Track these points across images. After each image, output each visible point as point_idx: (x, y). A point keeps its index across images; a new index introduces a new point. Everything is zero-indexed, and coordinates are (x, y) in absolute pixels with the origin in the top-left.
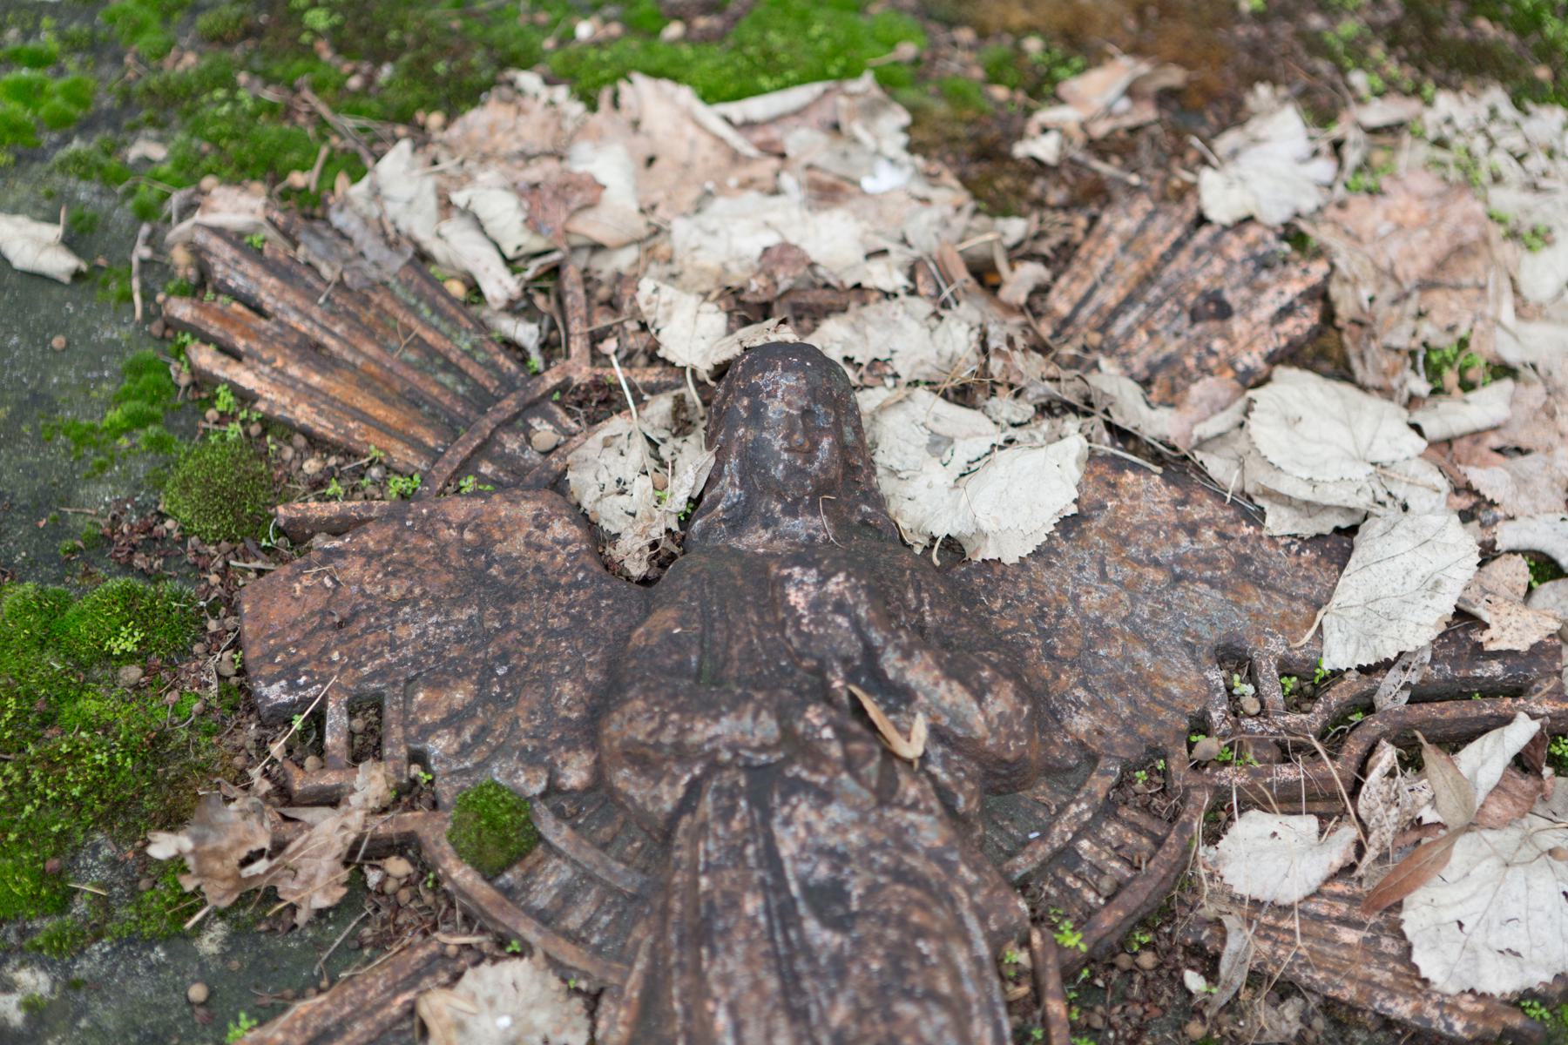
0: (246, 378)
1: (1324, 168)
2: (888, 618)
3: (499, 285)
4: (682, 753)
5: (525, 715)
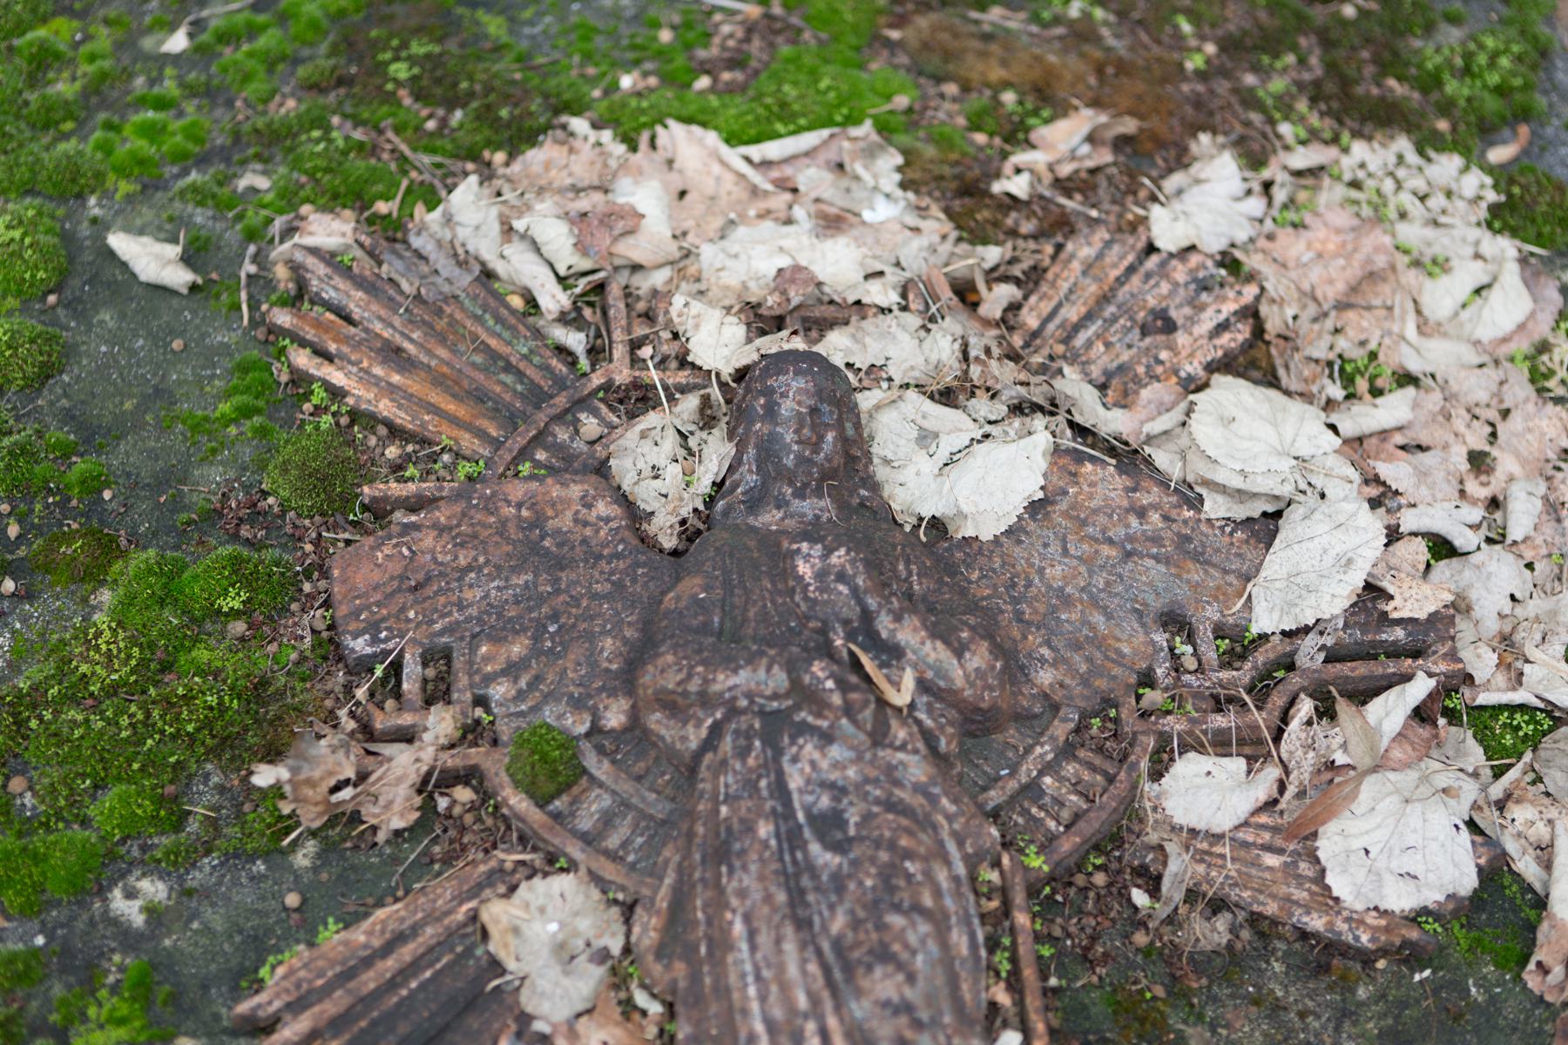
0: (337, 378)
1: (1256, 205)
2: (882, 587)
4: (706, 700)
5: (572, 666)
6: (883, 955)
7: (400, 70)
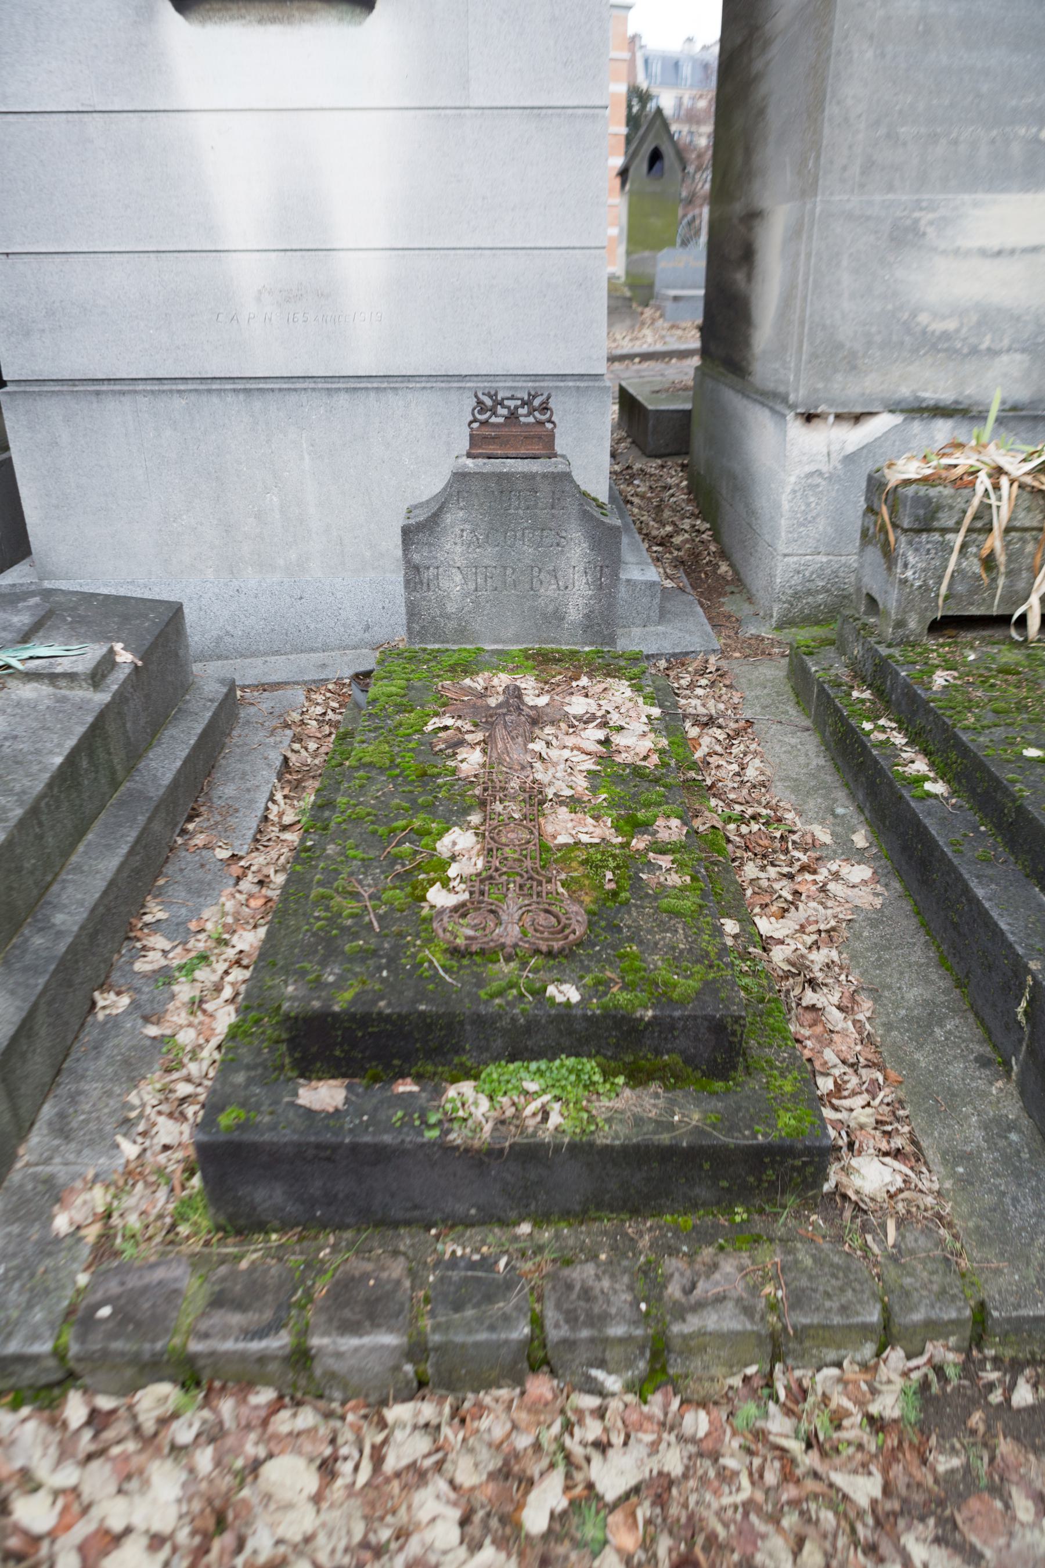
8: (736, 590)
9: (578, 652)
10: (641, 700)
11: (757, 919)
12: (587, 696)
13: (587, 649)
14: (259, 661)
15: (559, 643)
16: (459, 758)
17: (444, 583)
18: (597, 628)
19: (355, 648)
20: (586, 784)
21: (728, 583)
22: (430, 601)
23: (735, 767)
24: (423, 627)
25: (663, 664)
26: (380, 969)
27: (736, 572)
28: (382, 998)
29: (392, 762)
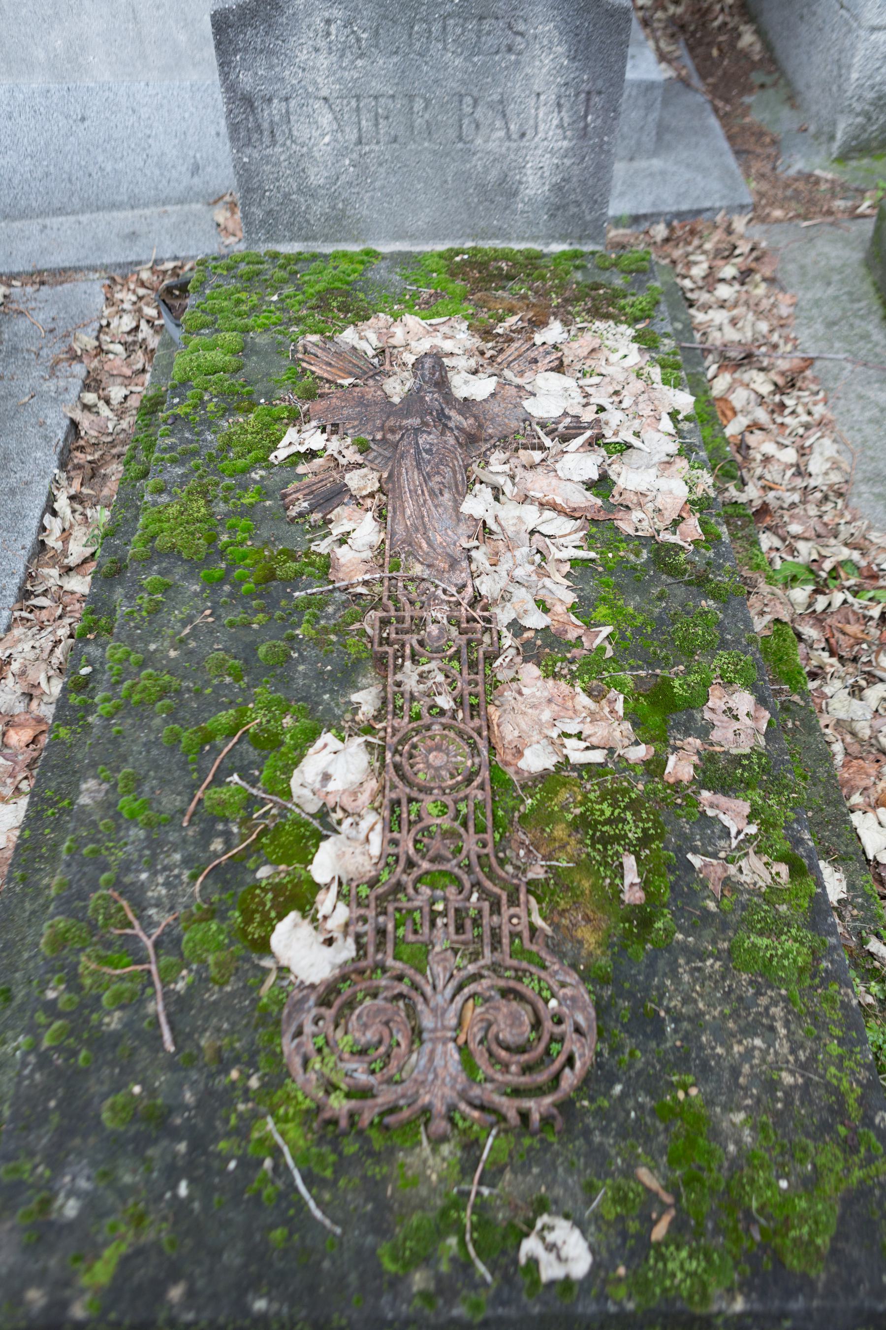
0: (313, 368)
1: (565, 335)
2: (447, 403)
3: (371, 353)
4: (401, 428)
5: (369, 427)
6: (438, 473)
7: (335, 304)
8: (768, 80)
9: (541, 256)
10: (656, 373)
11: (856, 819)
12: (560, 368)
13: (557, 248)
14: (32, 226)
15: (507, 237)
16: (337, 530)
17: (300, 130)
18: (573, 210)
19: (181, 201)
20: (570, 598)
21: (755, 66)
22: (277, 164)
23: (790, 455)
24: (269, 213)
25: (660, 231)
26: (172, 1177)
27: (768, 47)
28: (174, 1277)
29: (212, 541)
